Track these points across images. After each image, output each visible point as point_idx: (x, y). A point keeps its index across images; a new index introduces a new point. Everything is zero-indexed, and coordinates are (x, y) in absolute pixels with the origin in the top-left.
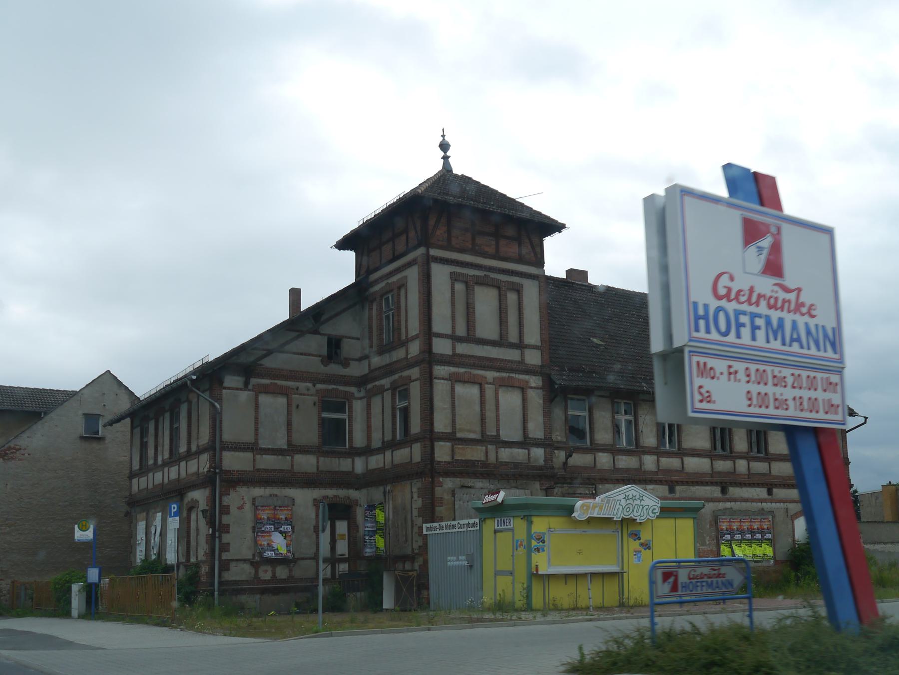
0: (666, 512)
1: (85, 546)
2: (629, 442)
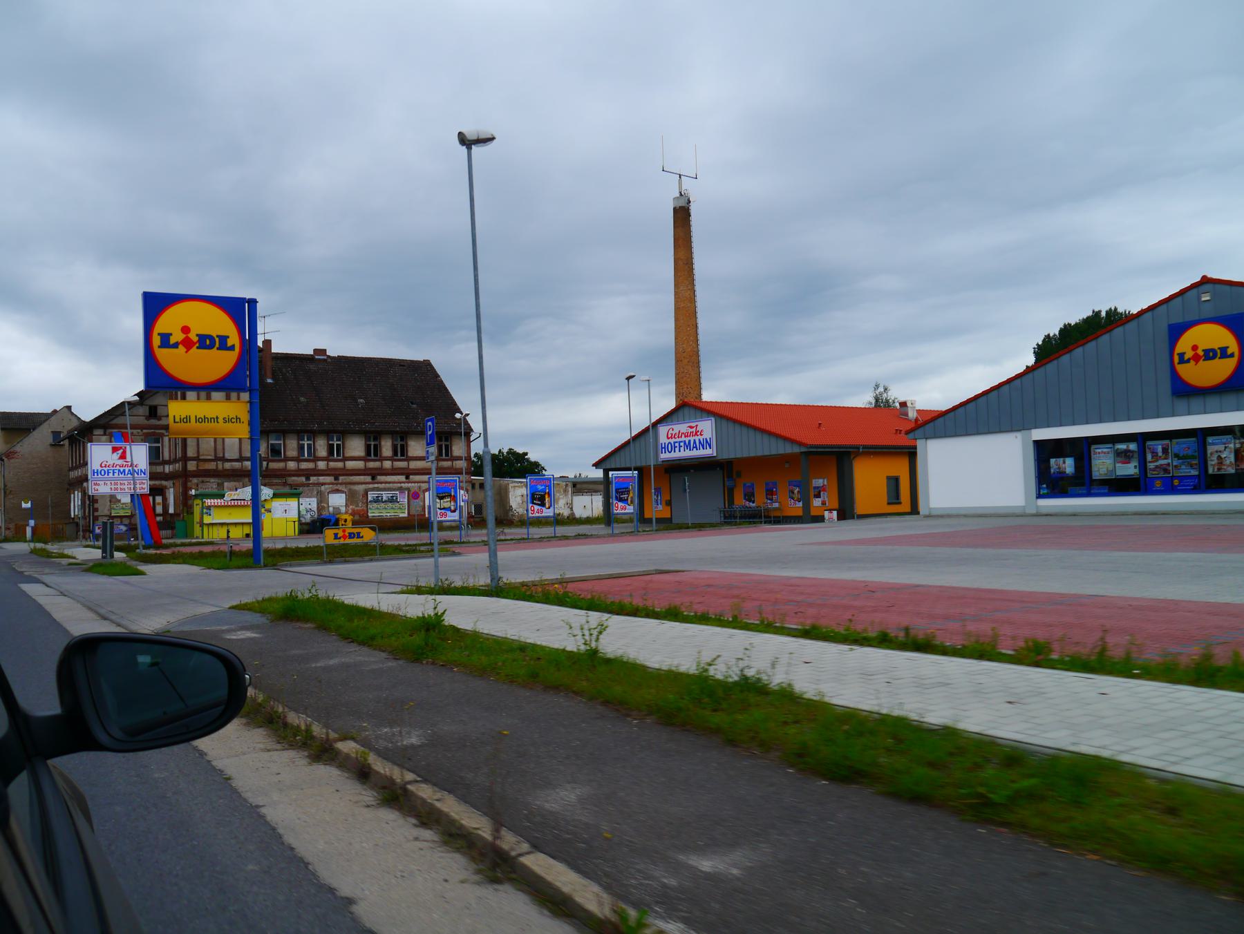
0: (275, 496)
1: (26, 509)
2: (309, 454)
